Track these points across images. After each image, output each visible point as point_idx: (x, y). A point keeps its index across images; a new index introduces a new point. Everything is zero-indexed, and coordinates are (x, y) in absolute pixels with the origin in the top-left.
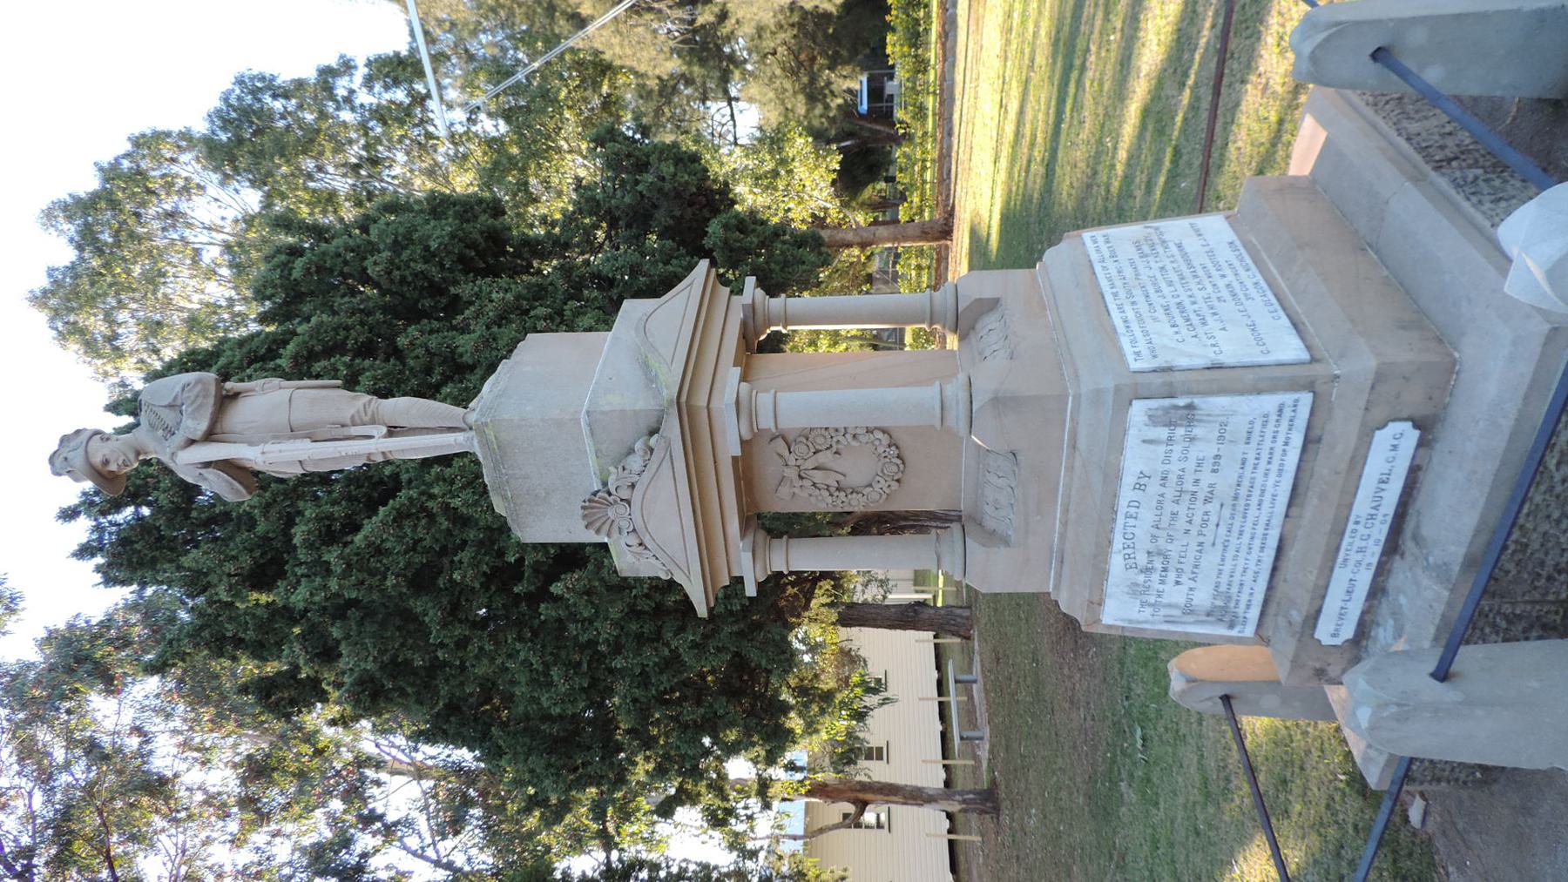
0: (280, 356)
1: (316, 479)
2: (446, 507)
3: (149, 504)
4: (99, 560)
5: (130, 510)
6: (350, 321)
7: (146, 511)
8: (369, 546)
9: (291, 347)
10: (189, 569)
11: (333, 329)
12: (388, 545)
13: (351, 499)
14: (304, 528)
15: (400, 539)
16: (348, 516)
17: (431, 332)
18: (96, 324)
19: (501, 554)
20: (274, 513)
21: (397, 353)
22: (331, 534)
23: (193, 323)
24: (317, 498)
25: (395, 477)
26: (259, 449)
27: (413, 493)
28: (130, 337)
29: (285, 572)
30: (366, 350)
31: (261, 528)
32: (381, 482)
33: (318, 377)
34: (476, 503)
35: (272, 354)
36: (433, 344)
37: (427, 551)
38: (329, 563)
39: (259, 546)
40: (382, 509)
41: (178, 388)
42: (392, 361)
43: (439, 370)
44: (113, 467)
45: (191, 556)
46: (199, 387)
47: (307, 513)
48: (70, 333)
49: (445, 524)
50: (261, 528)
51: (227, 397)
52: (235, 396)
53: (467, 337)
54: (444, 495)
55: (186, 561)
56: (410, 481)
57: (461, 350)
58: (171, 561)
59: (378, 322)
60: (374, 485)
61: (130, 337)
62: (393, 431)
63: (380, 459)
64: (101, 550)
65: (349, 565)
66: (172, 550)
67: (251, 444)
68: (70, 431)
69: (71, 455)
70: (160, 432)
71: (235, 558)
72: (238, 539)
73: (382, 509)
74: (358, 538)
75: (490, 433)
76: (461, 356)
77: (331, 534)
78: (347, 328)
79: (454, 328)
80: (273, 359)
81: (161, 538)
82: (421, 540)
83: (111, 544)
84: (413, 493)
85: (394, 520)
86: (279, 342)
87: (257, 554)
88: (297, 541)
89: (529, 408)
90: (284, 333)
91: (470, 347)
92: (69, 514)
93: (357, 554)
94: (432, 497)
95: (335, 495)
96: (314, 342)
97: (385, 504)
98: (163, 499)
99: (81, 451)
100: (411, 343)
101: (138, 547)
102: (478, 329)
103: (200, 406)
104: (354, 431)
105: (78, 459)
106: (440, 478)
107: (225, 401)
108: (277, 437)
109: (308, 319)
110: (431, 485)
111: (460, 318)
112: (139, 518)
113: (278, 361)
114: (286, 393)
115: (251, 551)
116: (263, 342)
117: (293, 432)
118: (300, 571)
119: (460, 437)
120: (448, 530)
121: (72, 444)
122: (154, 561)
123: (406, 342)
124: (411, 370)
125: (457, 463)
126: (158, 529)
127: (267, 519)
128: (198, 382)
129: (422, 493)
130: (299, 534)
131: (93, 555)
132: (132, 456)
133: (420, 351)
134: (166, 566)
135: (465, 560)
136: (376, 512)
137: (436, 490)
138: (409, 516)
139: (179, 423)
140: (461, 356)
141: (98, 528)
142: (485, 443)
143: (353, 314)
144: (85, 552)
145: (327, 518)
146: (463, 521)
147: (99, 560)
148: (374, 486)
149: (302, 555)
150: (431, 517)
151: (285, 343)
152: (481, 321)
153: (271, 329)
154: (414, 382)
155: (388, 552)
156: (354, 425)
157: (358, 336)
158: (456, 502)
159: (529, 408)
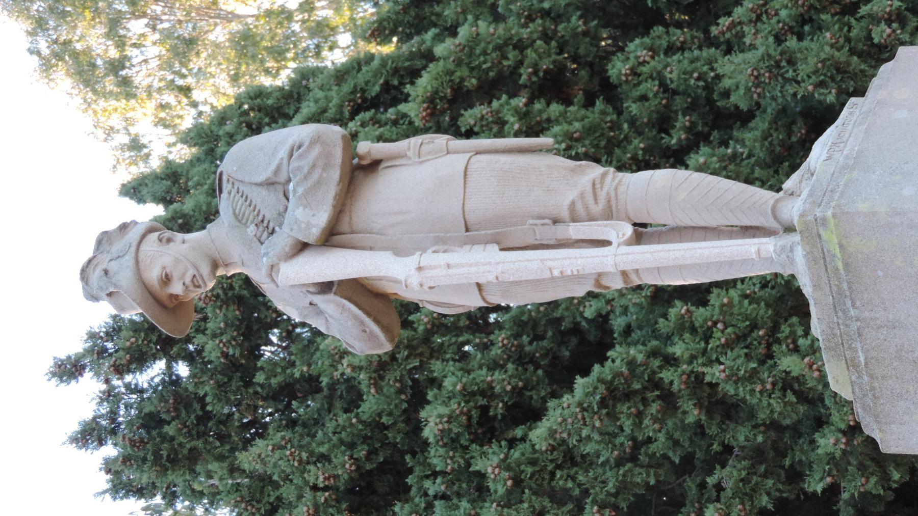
0: (406, 98)
1: (463, 322)
2: (697, 382)
3: (190, 358)
4: (110, 450)
5: (160, 365)
6: (525, 33)
7: (183, 369)
8: (553, 449)
9: (425, 83)
10: (251, 475)
11: (498, 48)
12: (589, 449)
13: (522, 359)
14: (444, 410)
15: (609, 437)
16: (517, 392)
17: (670, 50)
18: (93, 39)
19: (795, 475)
20: (391, 377)
21: (608, 91)
22: (492, 421)
23: (246, 44)
24: (465, 356)
25: (602, 320)
26: (412, 261)
27: (637, 353)
28: (147, 59)
29: (408, 488)
30: (553, 86)
31: (370, 405)
32: (576, 329)
33: (469, 134)
34: (752, 376)
35: (392, 94)
36: (673, 75)
37: (657, 462)
38: (482, 476)
39: (365, 439)
40: (580, 381)
41: (283, 153)
42: (599, 104)
43: (682, 121)
44: (177, 288)
45: (254, 450)
46: (317, 150)
47: (448, 383)
48: (59, 57)
49: (693, 414)
50: (370, 405)
51: (360, 168)
52: (374, 166)
53: (738, 58)
54: (693, 358)
55: (246, 459)
56: (628, 330)
57: (727, 83)
58: (221, 458)
59: (575, 35)
60: (566, 340)
61: (147, 59)
62: (642, 232)
63: (618, 284)
64: (113, 432)
65: (518, 482)
66: (222, 438)
67: (399, 251)
68: (112, 225)
69: (113, 266)
70: (251, 229)
71: (324, 458)
72: (330, 426)
73: (580, 381)
74: (539, 434)
75: (831, 239)
76: (726, 94)
77: (492, 421)
78: (520, 46)
79: (711, 42)
80: (395, 102)
81: (206, 416)
82: (650, 440)
83: (130, 423)
84: (637, 353)
85: (603, 403)
86: (404, 73)
87: (361, 452)
88: (430, 432)
89: (908, 191)
90: (412, 56)
91: (744, 78)
92: (68, 370)
93: (533, 462)
94: (670, 361)
95: (496, 351)
96: (463, 72)
97: (586, 373)
98: (212, 350)
99: (129, 260)
100: (634, 72)
101: (170, 430)
102: (761, 42)
103: (318, 183)
104: (575, 231)
105: (125, 277)
106: (686, 327)
107: (359, 171)
108: (443, 241)
109: (452, 31)
110: (668, 339)
111: (724, 22)
112: (172, 381)
113: (403, 107)
114: (459, 161)
115: (352, 446)
116: (377, 74)
117: (470, 232)
118: (434, 487)
119: (768, 245)
120: (699, 425)
121: (117, 248)
122: (193, 457)
123: (625, 69)
124: (632, 122)
125: (716, 299)
126: (202, 400)
127: (379, 390)
128: (316, 140)
129: (654, 354)
130: (433, 419)
131: (101, 442)
132: (205, 270)
133: (650, 87)
134: (214, 466)
135: (729, 484)
136: (570, 388)
137: (678, 349)
138: (628, 396)
139: (282, 214)
140: (726, 94)
141: (110, 395)
142: (820, 258)
143: (530, 19)
144: (90, 435)
145: (483, 393)
146: (726, 409)
147: (110, 450)
148: (563, 336)
149: (437, 458)
150: (669, 399)
151: (414, 74)
152: (765, 28)
153: (388, 49)
154: (638, 144)
155: (587, 462)
156: (575, 219)
157: (540, 59)
158: (715, 373)
159: (908, 191)
